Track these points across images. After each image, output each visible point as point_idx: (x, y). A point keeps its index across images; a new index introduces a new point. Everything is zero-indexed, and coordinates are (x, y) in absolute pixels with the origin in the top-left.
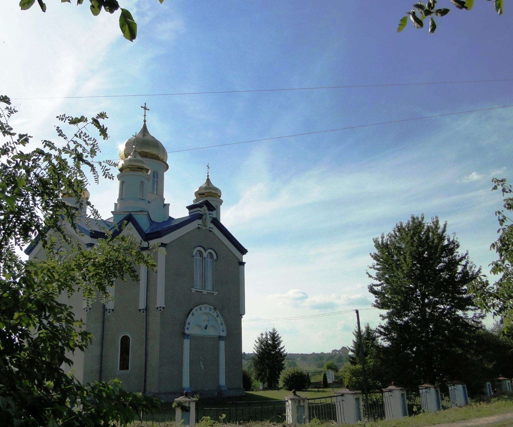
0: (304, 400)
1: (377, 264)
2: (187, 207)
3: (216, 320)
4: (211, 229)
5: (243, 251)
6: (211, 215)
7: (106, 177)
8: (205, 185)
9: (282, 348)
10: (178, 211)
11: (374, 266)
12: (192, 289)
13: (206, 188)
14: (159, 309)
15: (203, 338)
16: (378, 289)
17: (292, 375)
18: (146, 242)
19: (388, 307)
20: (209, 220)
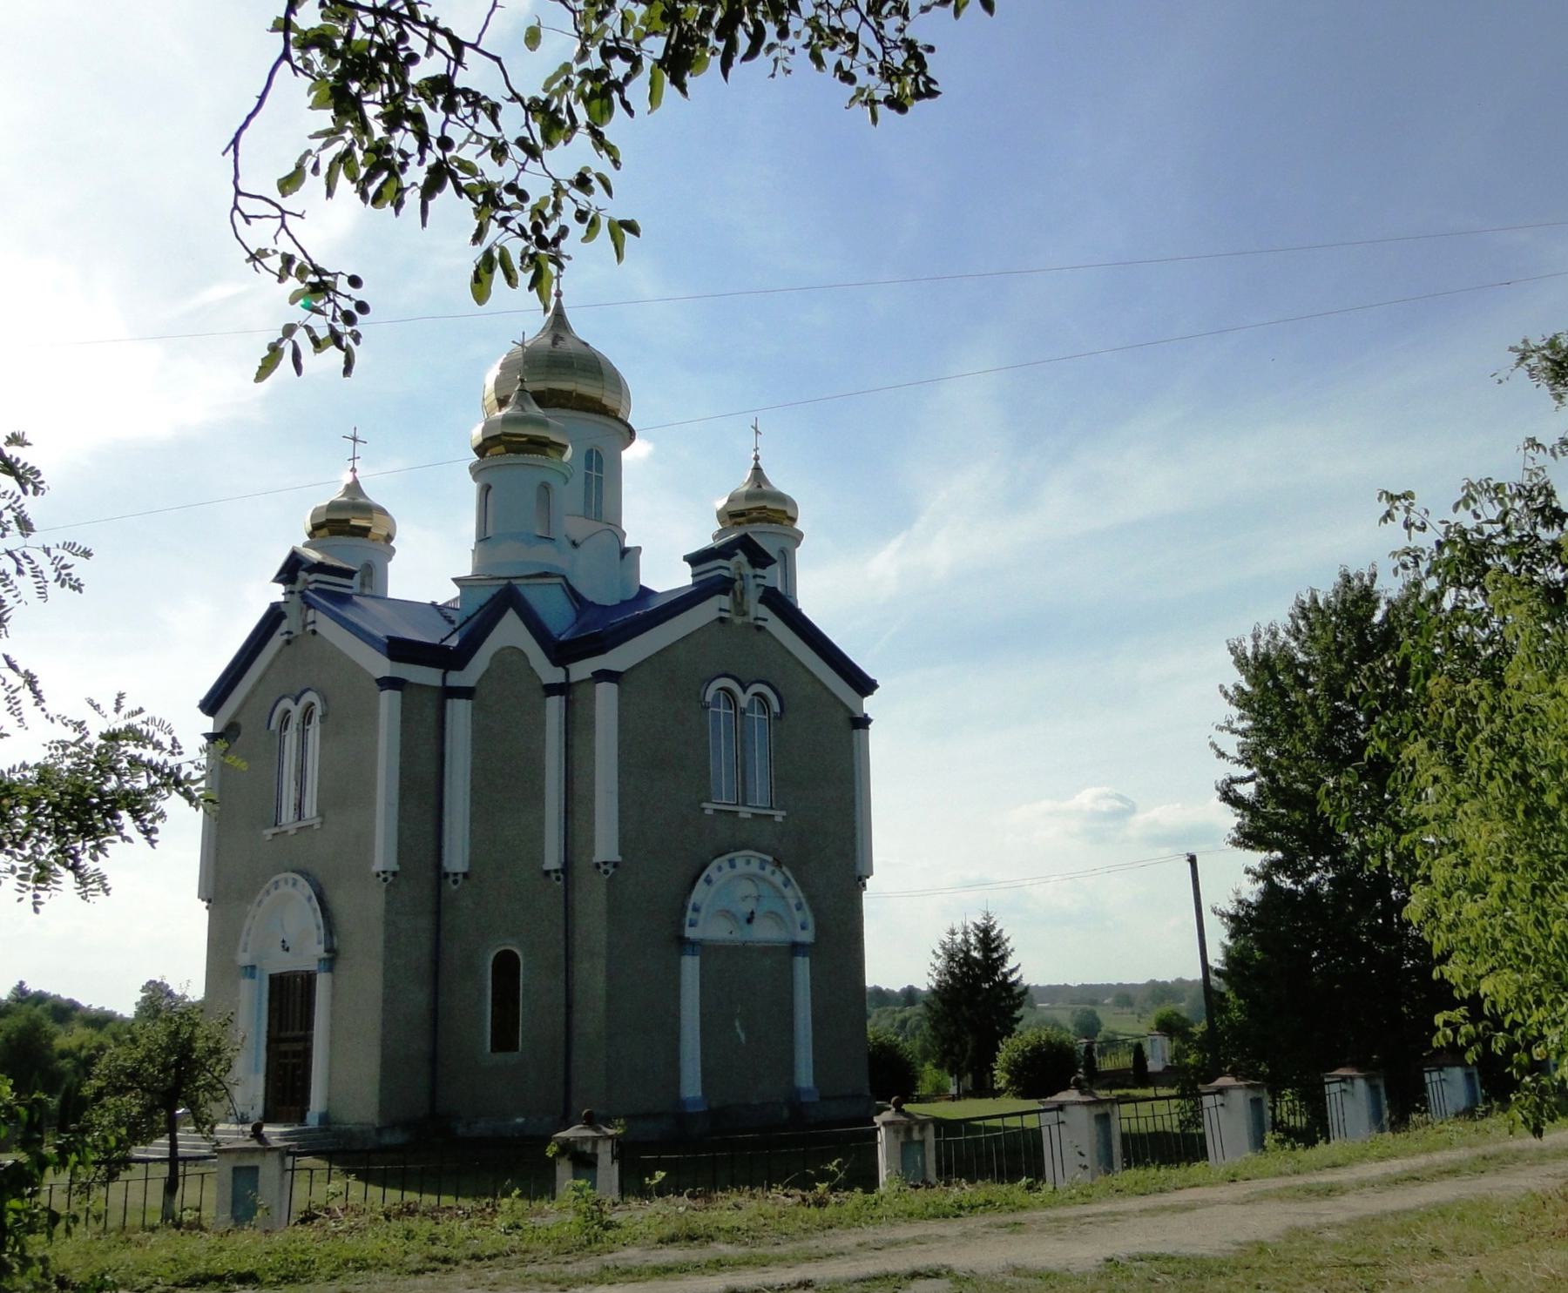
0: (923, 1125)
1: (1242, 718)
2: (686, 558)
4: (760, 623)
5: (865, 685)
7: (62, 585)
9: (1012, 971)
10: (665, 572)
11: (1230, 723)
12: (705, 805)
13: (749, 496)
14: (603, 867)
16: (1247, 790)
17: (1032, 1050)
18: (561, 669)
19: (1268, 846)
20: (753, 596)
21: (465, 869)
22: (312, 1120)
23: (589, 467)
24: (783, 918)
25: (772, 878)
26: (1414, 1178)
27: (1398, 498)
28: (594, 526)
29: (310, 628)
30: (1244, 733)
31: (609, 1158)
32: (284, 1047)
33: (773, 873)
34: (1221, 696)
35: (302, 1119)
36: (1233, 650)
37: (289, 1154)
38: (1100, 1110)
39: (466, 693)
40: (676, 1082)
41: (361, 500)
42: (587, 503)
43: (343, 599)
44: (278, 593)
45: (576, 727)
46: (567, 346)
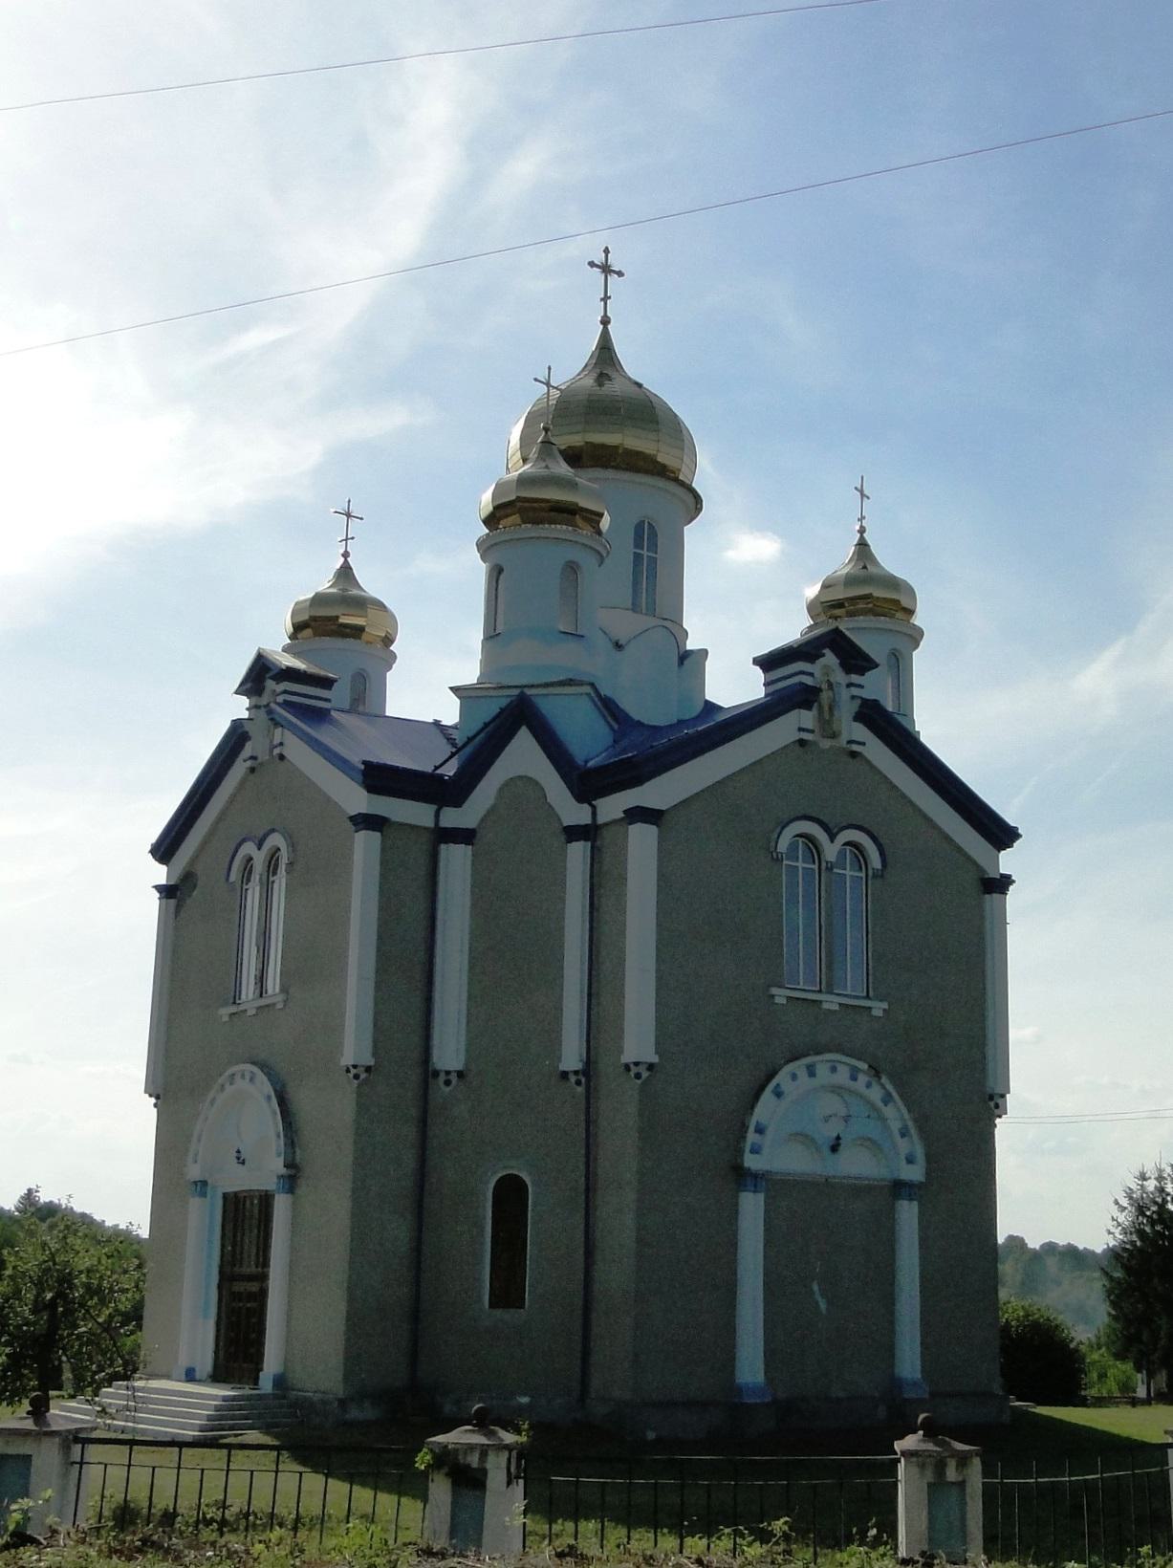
2: (757, 661)
3: (883, 1119)
4: (855, 748)
5: (1002, 835)
6: (855, 691)
8: (845, 571)
10: (733, 683)
12: (774, 991)
13: (850, 581)
15: (825, 1187)
20: (846, 710)
21: (460, 1067)
22: (266, 1384)
23: (638, 544)
24: (880, 1146)
25: (866, 1092)
29: (276, 751)
31: (503, 1476)
32: (239, 1287)
33: (869, 1085)
35: (255, 1381)
37: (77, 1440)
39: (466, 836)
41: (355, 592)
43: (318, 715)
46: (615, 388)
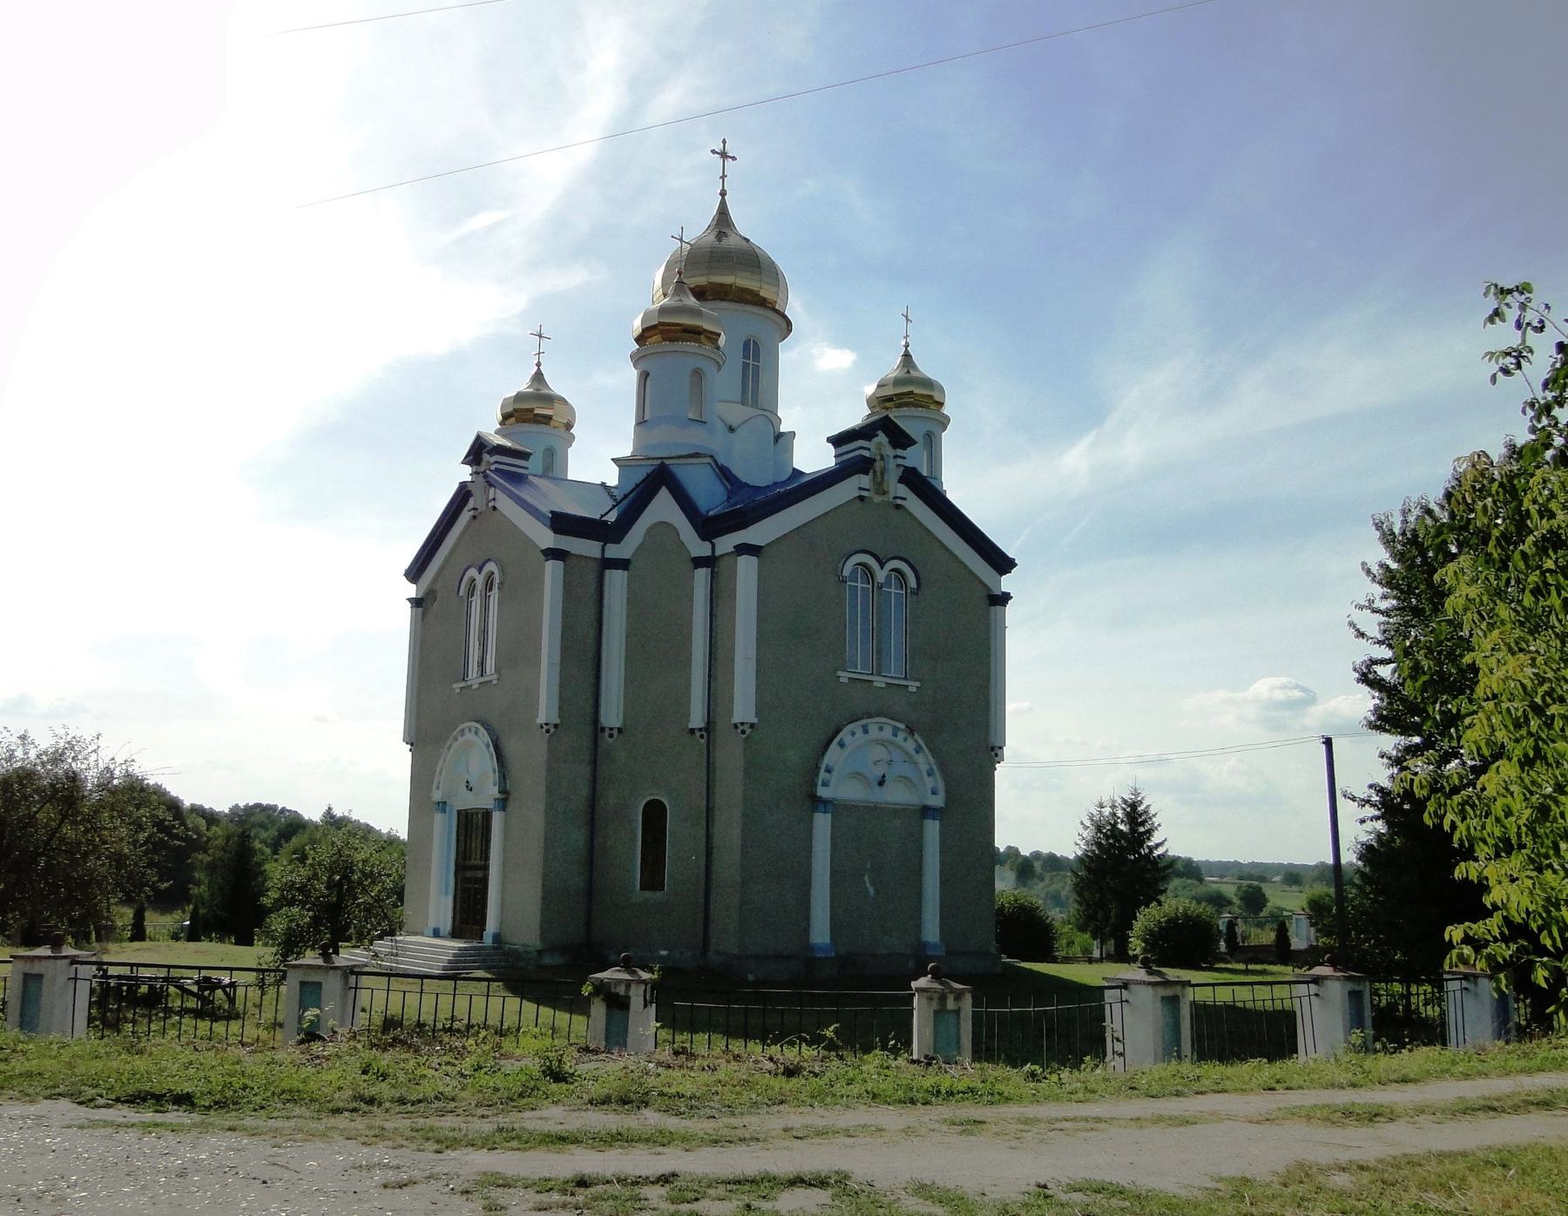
1: (1384, 597)
2: (829, 440)
5: (1003, 564)
6: (900, 461)
9: (1158, 846)
10: (813, 456)
12: (840, 673)
13: (897, 382)
15: (874, 810)
16: (1385, 672)
17: (1168, 922)
19: (1406, 730)
22: (488, 939)
23: (746, 355)
26: (1491, 1108)
27: (1510, 292)
28: (748, 411)
30: (1386, 613)
32: (469, 874)
34: (1363, 574)
36: (1378, 526)
37: (353, 973)
38: (1169, 992)
39: (623, 564)
40: (918, 927)
41: (545, 391)
42: (744, 392)
44: (465, 474)
45: (719, 597)
46: (731, 242)
